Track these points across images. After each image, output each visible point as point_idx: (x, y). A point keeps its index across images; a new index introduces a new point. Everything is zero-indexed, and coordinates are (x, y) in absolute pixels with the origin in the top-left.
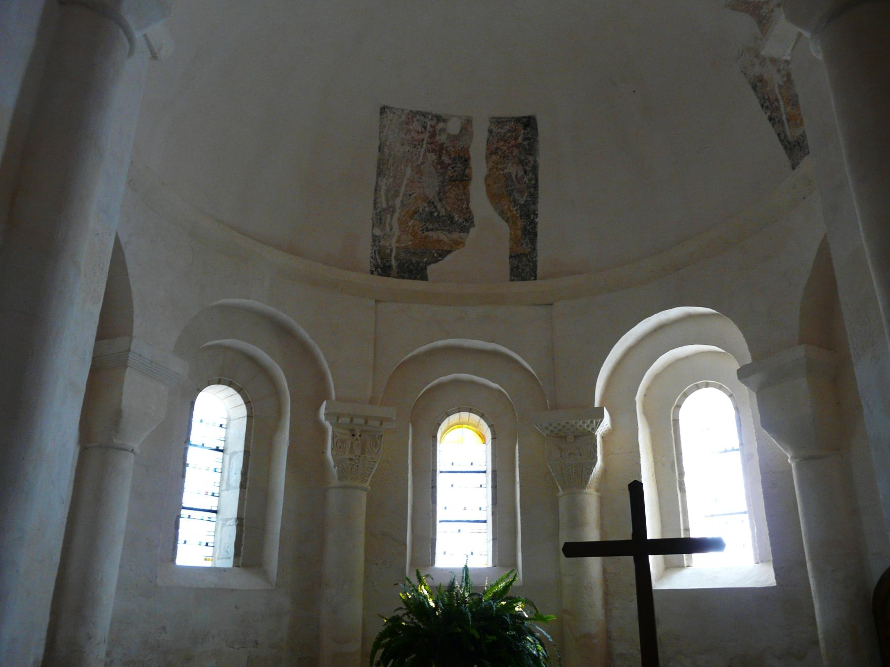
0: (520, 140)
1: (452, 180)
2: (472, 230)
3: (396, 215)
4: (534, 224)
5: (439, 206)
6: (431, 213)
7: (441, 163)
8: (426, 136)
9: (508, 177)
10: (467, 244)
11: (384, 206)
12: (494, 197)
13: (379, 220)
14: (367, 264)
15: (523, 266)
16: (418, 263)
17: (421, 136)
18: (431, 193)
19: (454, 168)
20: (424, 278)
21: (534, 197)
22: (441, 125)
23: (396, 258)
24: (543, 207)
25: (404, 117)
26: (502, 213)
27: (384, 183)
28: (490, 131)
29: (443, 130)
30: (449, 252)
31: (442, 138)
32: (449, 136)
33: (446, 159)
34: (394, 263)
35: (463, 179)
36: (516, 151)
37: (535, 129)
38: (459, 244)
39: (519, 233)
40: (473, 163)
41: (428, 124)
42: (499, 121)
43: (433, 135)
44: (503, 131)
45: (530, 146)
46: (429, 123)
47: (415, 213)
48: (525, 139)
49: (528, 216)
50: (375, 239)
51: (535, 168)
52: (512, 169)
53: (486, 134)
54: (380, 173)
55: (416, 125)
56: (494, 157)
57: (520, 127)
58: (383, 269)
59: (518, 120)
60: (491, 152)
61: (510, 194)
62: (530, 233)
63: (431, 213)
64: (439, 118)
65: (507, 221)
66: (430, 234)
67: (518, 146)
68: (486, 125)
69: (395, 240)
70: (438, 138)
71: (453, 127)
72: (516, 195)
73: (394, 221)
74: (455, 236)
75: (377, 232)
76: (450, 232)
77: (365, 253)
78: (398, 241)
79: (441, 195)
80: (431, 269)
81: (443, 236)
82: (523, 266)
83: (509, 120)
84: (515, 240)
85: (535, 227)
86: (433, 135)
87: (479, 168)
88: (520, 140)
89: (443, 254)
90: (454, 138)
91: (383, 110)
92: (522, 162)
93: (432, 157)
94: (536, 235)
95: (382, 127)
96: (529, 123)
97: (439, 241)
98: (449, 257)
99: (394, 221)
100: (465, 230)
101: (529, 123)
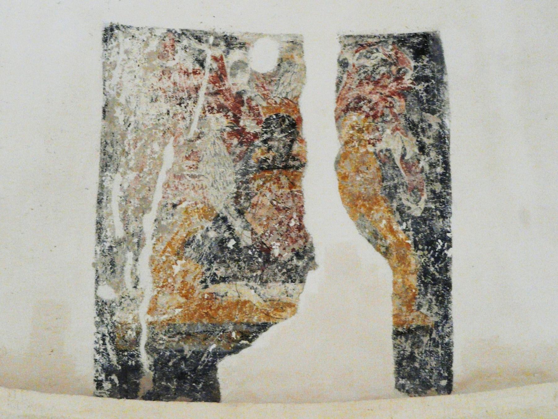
0: (407, 81)
1: (264, 167)
2: (311, 276)
3: (146, 253)
4: (442, 261)
5: (238, 225)
6: (222, 243)
7: (239, 133)
8: (204, 80)
9: (385, 158)
10: (302, 306)
11: (120, 233)
12: (357, 203)
13: (109, 265)
14: (87, 368)
15: (423, 362)
16: (197, 355)
17: (193, 81)
18: (221, 199)
19: (269, 144)
20: (212, 394)
21: (442, 201)
22: (236, 55)
23: (151, 349)
24: (462, 224)
25: (154, 45)
26: (375, 238)
27: (116, 184)
28: (343, 64)
29: (240, 65)
30: (264, 327)
31: (238, 82)
32: (255, 76)
33: (249, 124)
34: (146, 360)
35: (289, 166)
36: (399, 104)
37: (438, 58)
38: (283, 307)
39: (413, 280)
40: (307, 130)
41: (208, 61)
42: (362, 44)
43: (219, 76)
44: (369, 63)
45: (430, 94)
46: (209, 53)
47: (187, 243)
48: (417, 80)
49: (430, 243)
50: (102, 308)
51: (442, 140)
52: (395, 142)
53: (334, 70)
54: (107, 164)
55: (183, 59)
56: (354, 117)
57: (407, 55)
58: (122, 379)
59: (402, 41)
60: (347, 107)
61: (391, 196)
62: (436, 281)
63: (222, 243)
64: (230, 42)
65: (386, 254)
66: (222, 288)
67: (403, 93)
68: (335, 50)
69: (149, 306)
70: (229, 82)
71: (263, 58)
72: (405, 198)
73: (141, 268)
74: (275, 290)
75: (107, 293)
76: (264, 283)
77: (83, 353)
78: (150, 311)
79: (242, 200)
80: (228, 370)
81: (244, 291)
82: (423, 362)
83: (383, 40)
84: (406, 300)
85: (445, 269)
86: (219, 76)
87: (321, 139)
88: (407, 81)
89: (249, 334)
90: (266, 81)
91: (109, 33)
92: (413, 127)
93: (219, 122)
94: (448, 284)
95: (108, 67)
96: (425, 46)
97: (241, 304)
98: (263, 339)
99: (141, 268)
100: (294, 275)
101: (425, 46)
